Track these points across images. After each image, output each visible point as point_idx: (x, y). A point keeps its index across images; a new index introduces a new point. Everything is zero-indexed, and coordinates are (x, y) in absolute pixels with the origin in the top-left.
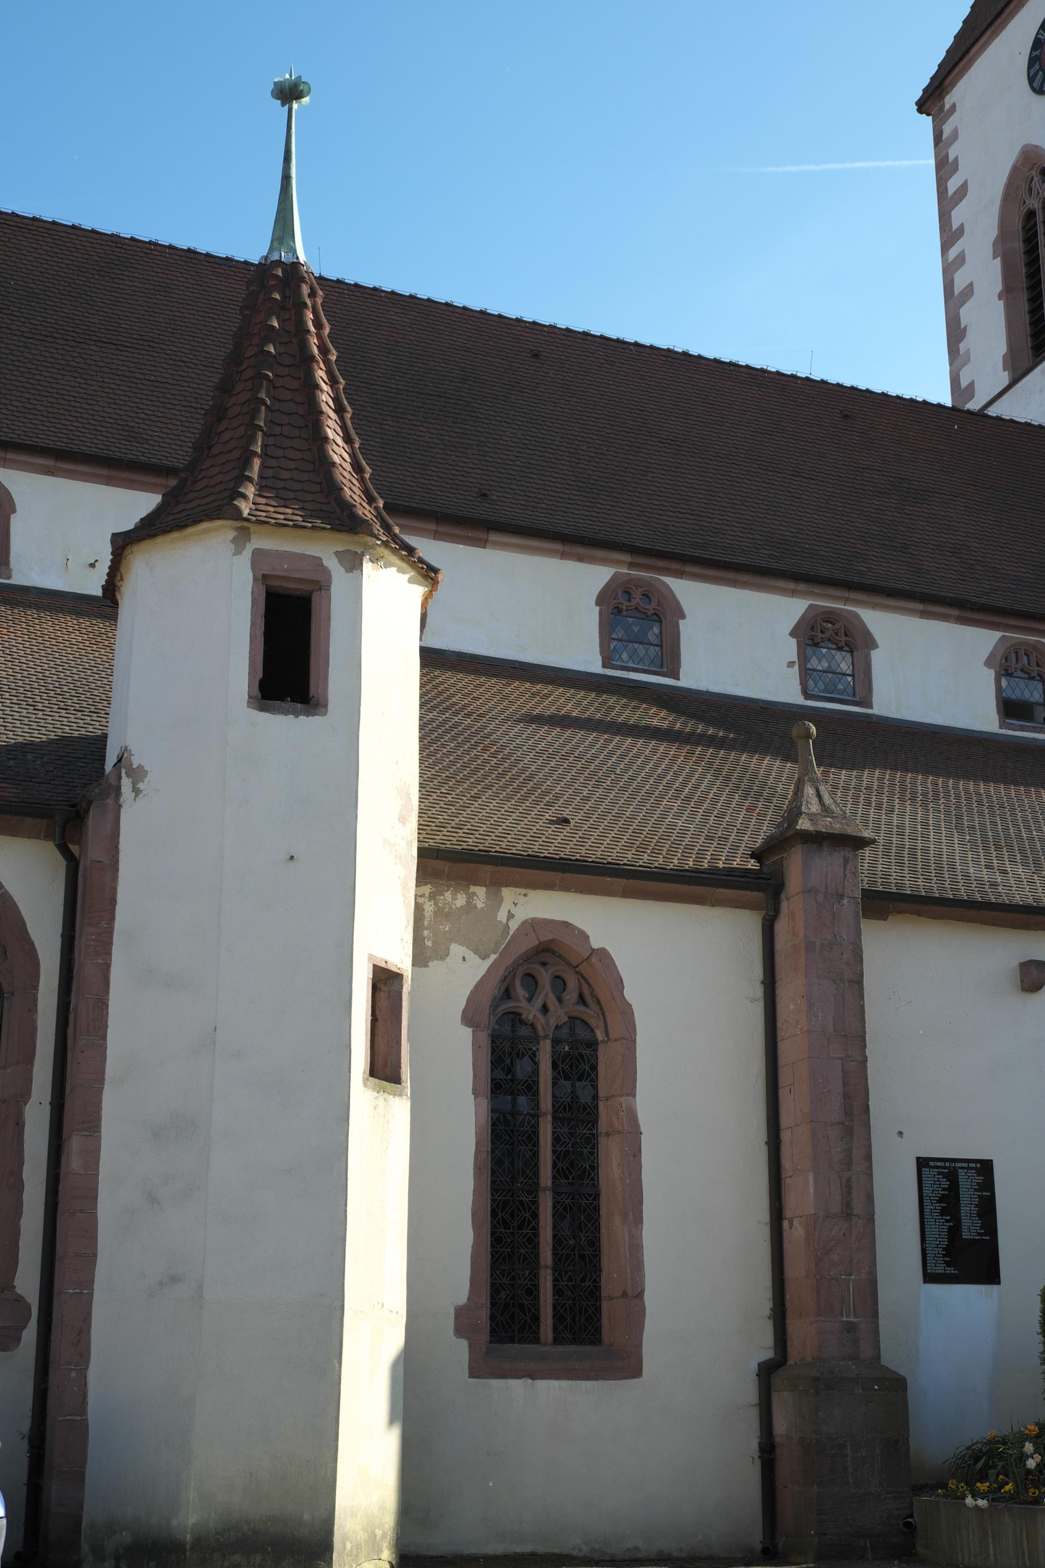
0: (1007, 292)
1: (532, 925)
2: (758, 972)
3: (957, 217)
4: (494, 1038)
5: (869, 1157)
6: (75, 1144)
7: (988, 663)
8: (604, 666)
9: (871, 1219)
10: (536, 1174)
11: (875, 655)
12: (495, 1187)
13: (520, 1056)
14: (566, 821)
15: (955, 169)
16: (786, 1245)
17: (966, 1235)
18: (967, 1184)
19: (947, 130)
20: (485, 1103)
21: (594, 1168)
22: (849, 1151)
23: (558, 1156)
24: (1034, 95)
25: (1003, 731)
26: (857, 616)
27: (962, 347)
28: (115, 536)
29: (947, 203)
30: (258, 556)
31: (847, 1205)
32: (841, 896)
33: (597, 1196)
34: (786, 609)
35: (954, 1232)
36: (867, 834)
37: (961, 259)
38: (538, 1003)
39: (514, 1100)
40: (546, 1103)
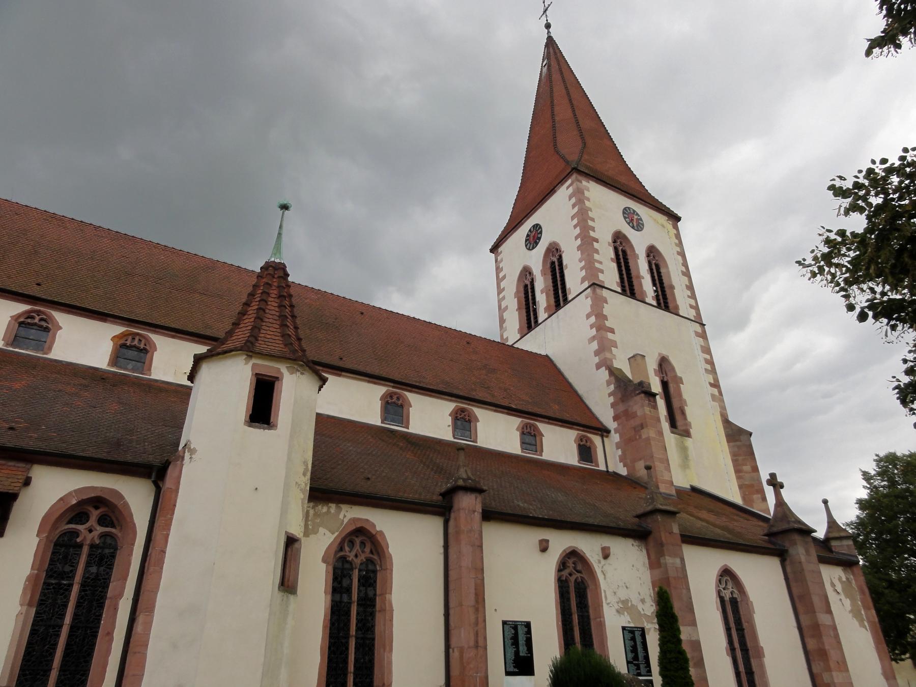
0: (519, 309)
1: (354, 520)
2: (442, 543)
3: (502, 285)
4: (335, 569)
5: (485, 621)
6: (141, 619)
7: (517, 429)
9: (486, 649)
10: (349, 630)
11: (478, 424)
12: (331, 636)
13: (345, 576)
14: (368, 479)
16: (451, 660)
17: (521, 654)
18: (521, 631)
19: (499, 258)
20: (329, 597)
21: (373, 626)
22: (477, 619)
23: (358, 621)
28: (195, 356)
29: (499, 280)
30: (254, 366)
31: (477, 642)
32: (474, 511)
33: (373, 639)
34: (448, 407)
35: (517, 653)
36: (485, 488)
37: (504, 298)
38: (353, 553)
39: (341, 597)
40: (355, 597)
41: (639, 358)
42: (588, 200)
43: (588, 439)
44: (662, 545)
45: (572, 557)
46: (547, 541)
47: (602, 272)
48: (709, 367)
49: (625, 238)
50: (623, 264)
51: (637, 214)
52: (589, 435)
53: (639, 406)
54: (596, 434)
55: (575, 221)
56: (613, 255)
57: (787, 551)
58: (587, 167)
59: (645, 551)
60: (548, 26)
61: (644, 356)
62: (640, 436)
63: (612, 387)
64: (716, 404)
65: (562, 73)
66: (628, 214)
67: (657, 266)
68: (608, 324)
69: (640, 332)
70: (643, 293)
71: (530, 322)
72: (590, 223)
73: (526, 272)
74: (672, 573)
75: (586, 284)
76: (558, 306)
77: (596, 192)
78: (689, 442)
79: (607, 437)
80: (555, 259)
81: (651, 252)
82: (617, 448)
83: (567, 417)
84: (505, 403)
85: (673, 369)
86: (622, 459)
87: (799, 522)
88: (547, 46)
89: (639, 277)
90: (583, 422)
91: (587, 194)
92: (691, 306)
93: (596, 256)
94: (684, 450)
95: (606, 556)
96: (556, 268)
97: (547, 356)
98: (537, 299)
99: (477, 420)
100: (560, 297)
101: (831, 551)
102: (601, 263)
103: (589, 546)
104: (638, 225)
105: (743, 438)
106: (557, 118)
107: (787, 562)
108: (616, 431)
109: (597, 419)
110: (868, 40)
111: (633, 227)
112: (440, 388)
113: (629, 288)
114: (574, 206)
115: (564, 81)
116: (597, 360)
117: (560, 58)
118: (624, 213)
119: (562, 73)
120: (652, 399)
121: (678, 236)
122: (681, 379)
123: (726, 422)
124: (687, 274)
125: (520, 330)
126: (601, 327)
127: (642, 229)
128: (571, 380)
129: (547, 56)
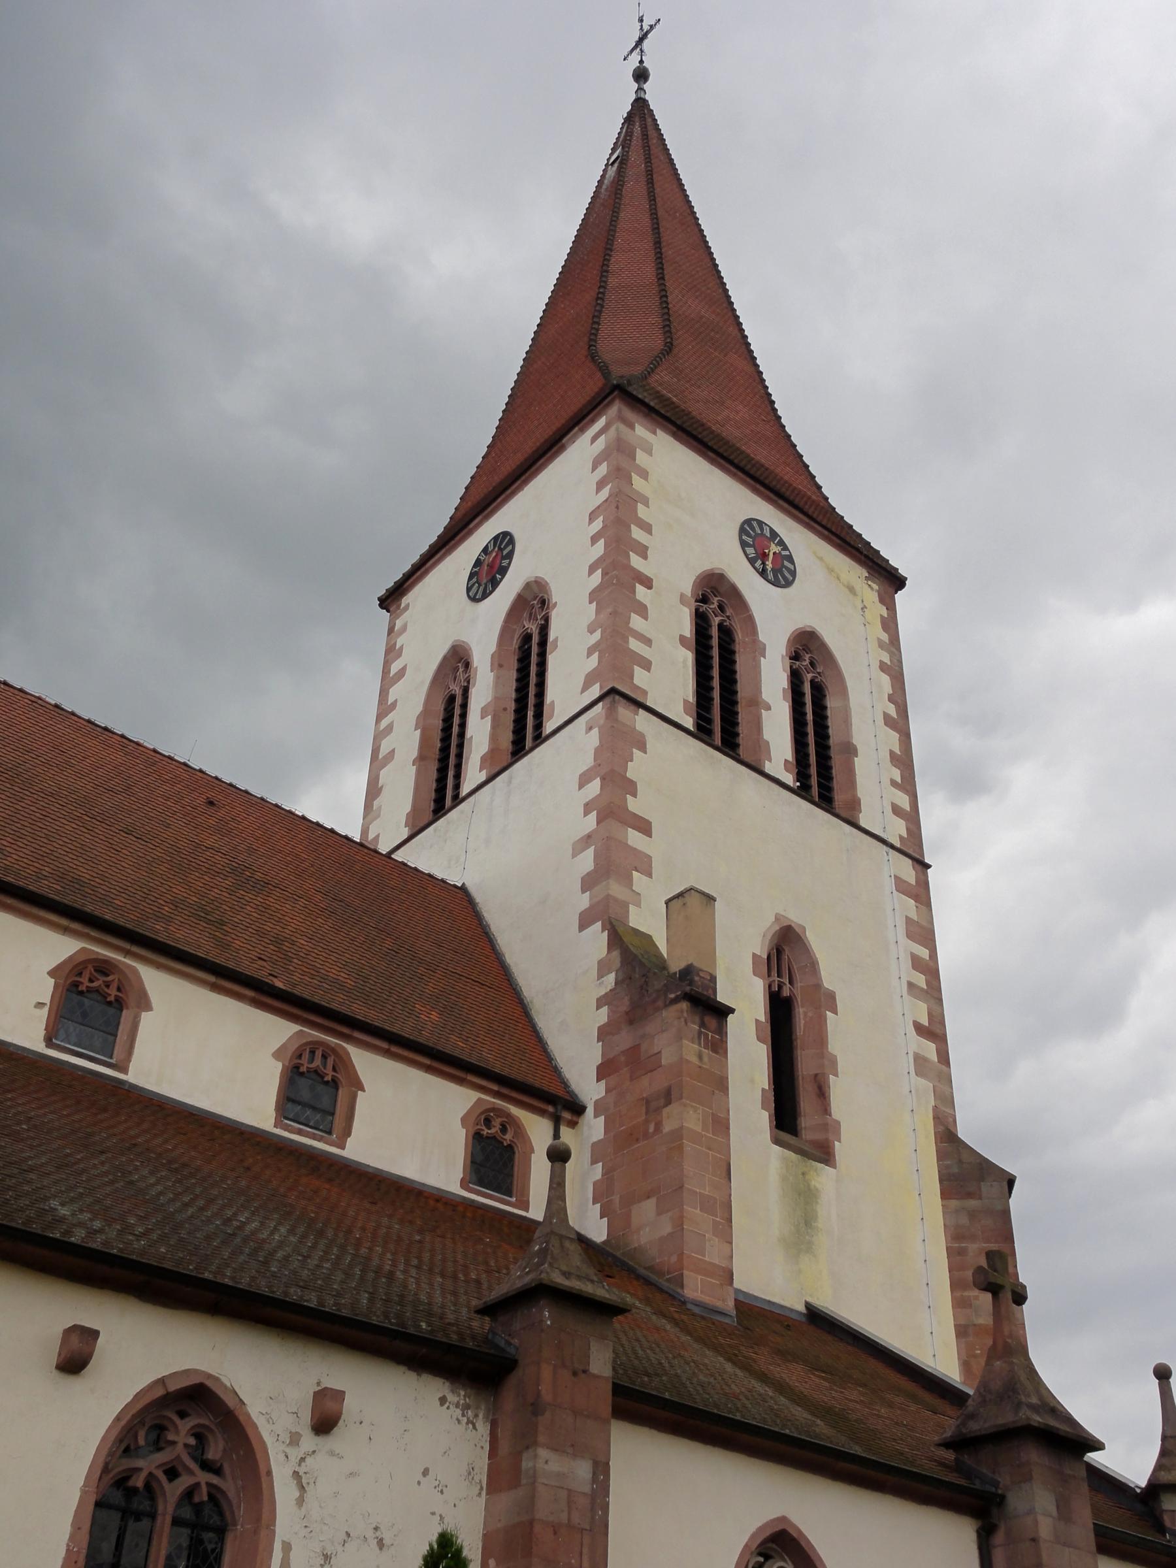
0: (421, 758)
3: (394, 693)
7: (277, 1055)
8: (275, 1126)
11: (145, 1016)
15: (399, 654)
19: (399, 624)
24: (469, 601)
25: (278, 1131)
26: (135, 972)
27: (376, 803)
29: (388, 680)
37: (390, 728)
41: (693, 900)
42: (644, 474)
43: (509, 1123)
44: (536, 1408)
45: (190, 1412)
46: (92, 1335)
47: (647, 665)
48: (921, 980)
49: (735, 594)
50: (813, 759)
51: (782, 543)
52: (515, 1111)
53: (673, 1038)
54: (541, 1112)
55: (598, 524)
56: (687, 628)
57: (1001, 1500)
58: (659, 396)
59: (483, 1429)
60: (641, 75)
61: (711, 899)
62: (658, 1128)
63: (610, 979)
64: (925, 1085)
65: (650, 182)
66: (753, 537)
67: (819, 691)
68: (633, 805)
69: (731, 848)
70: (762, 748)
71: (441, 794)
72: (637, 533)
73: (458, 660)
74: (547, 1509)
75: (595, 691)
76: (519, 750)
77: (667, 461)
78: (823, 1177)
79: (573, 1124)
80: (533, 628)
81: (807, 649)
82: (594, 1162)
83: (456, 1046)
84: (260, 970)
85: (813, 966)
86: (602, 1194)
87: (1055, 1409)
88: (629, 120)
89: (757, 703)
90: (498, 1067)
91: (641, 457)
92: (897, 810)
93: (636, 622)
94: (803, 1199)
95: (325, 1423)
96: (528, 655)
97: (463, 889)
98: (470, 732)
99: (144, 1003)
101: (1161, 1529)
102: (648, 642)
103: (265, 1379)
104: (780, 573)
105: (990, 1189)
106: (612, 281)
107: (999, 1538)
108: (599, 1109)
109: (556, 1071)
111: (763, 573)
112: (47, 888)
114: (600, 485)
115: (652, 198)
116: (584, 901)
117: (655, 150)
118: (742, 531)
119: (650, 182)
120: (712, 1022)
121: (890, 624)
122: (831, 996)
123: (948, 1138)
124: (899, 723)
126: (614, 803)
127: (788, 584)
128: (510, 958)
129: (624, 141)
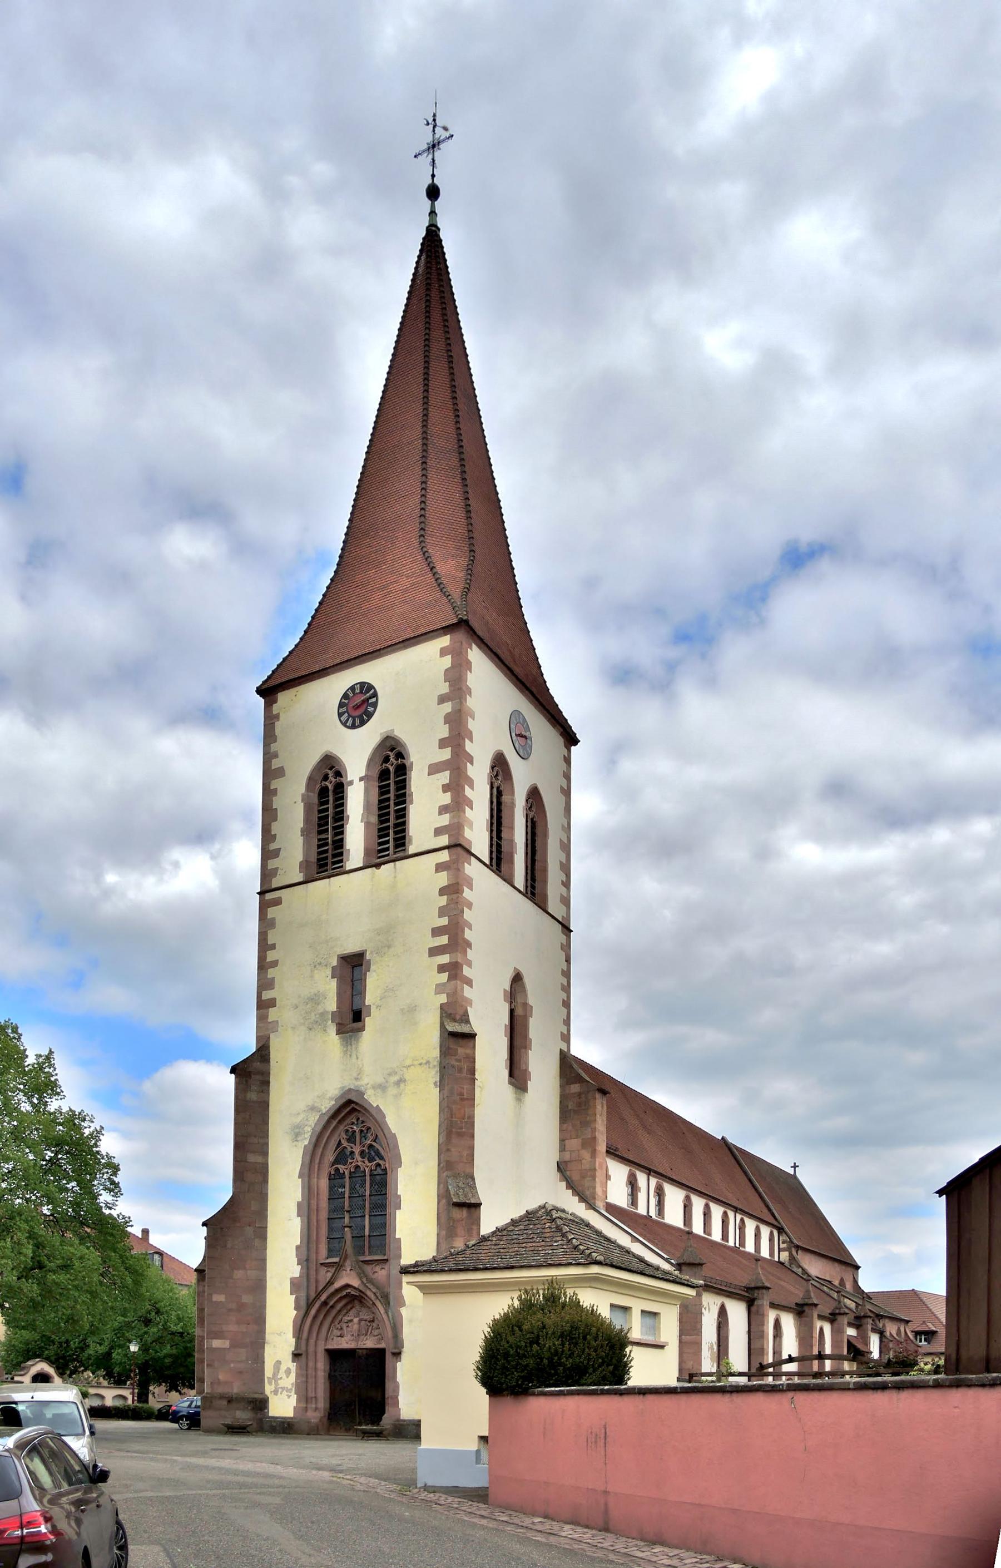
77: (483, 673)
96: (391, 770)
100: (391, 838)
110: (940, 1192)
113: (498, 861)
121: (568, 760)
125: (304, 865)
